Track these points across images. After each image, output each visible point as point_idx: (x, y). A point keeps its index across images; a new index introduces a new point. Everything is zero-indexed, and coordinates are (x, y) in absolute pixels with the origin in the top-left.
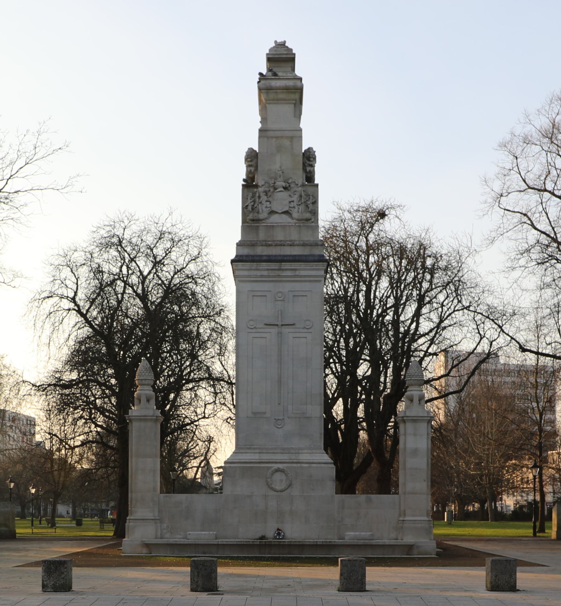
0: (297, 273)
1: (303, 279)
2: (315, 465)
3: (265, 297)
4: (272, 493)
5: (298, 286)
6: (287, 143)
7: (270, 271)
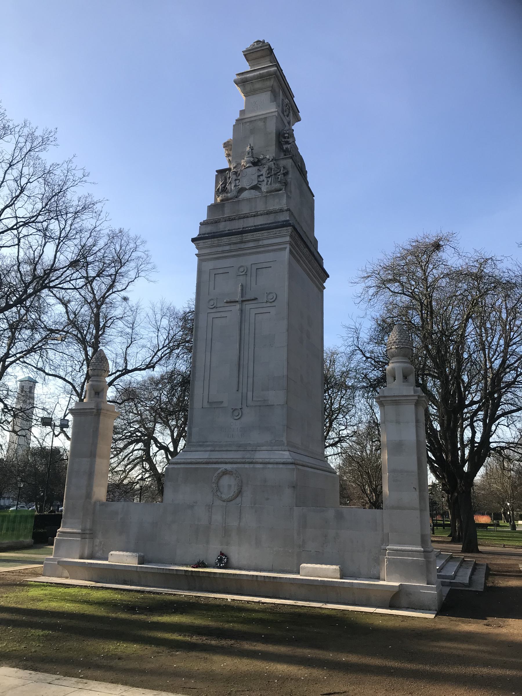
0: (261, 243)
1: (267, 249)
2: (270, 466)
4: (218, 502)
5: (261, 258)
7: (232, 246)
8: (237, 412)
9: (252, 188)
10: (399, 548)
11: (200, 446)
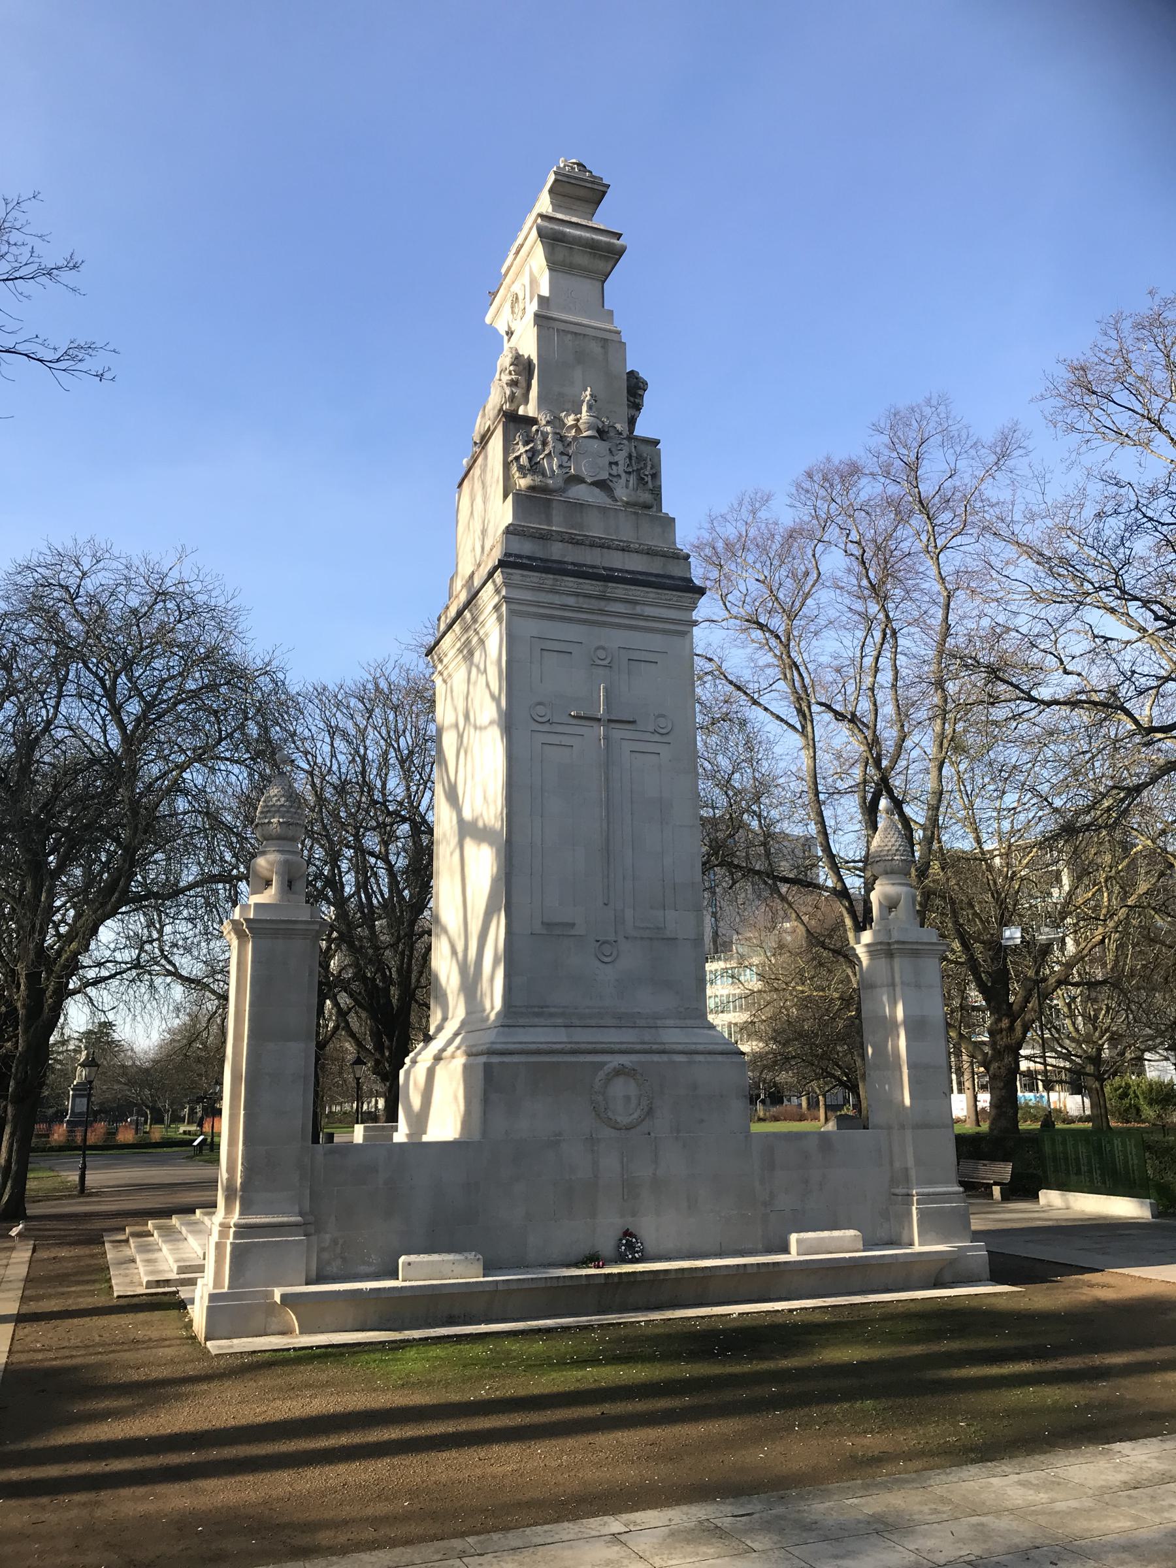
0: (639, 609)
1: (617, 620)
2: (700, 1058)
3: (566, 656)
4: (607, 1132)
5: (637, 640)
6: (596, 348)
7: (581, 599)
8: (605, 949)
9: (596, 484)
10: (931, 1190)
11: (538, 1015)
